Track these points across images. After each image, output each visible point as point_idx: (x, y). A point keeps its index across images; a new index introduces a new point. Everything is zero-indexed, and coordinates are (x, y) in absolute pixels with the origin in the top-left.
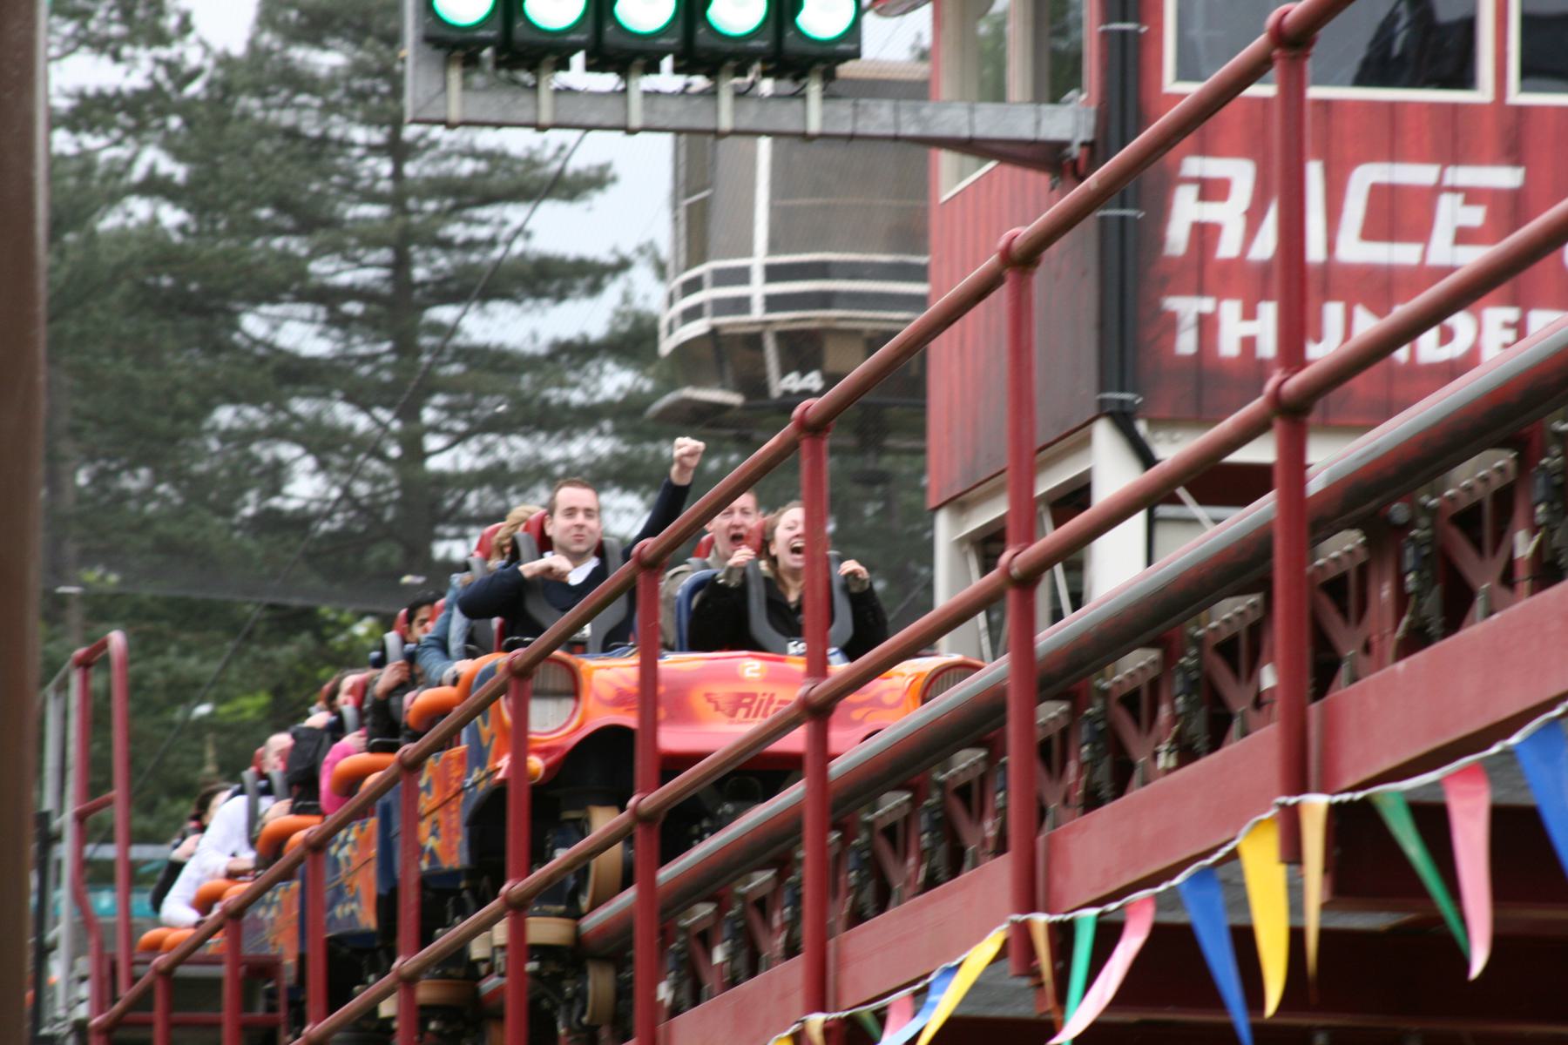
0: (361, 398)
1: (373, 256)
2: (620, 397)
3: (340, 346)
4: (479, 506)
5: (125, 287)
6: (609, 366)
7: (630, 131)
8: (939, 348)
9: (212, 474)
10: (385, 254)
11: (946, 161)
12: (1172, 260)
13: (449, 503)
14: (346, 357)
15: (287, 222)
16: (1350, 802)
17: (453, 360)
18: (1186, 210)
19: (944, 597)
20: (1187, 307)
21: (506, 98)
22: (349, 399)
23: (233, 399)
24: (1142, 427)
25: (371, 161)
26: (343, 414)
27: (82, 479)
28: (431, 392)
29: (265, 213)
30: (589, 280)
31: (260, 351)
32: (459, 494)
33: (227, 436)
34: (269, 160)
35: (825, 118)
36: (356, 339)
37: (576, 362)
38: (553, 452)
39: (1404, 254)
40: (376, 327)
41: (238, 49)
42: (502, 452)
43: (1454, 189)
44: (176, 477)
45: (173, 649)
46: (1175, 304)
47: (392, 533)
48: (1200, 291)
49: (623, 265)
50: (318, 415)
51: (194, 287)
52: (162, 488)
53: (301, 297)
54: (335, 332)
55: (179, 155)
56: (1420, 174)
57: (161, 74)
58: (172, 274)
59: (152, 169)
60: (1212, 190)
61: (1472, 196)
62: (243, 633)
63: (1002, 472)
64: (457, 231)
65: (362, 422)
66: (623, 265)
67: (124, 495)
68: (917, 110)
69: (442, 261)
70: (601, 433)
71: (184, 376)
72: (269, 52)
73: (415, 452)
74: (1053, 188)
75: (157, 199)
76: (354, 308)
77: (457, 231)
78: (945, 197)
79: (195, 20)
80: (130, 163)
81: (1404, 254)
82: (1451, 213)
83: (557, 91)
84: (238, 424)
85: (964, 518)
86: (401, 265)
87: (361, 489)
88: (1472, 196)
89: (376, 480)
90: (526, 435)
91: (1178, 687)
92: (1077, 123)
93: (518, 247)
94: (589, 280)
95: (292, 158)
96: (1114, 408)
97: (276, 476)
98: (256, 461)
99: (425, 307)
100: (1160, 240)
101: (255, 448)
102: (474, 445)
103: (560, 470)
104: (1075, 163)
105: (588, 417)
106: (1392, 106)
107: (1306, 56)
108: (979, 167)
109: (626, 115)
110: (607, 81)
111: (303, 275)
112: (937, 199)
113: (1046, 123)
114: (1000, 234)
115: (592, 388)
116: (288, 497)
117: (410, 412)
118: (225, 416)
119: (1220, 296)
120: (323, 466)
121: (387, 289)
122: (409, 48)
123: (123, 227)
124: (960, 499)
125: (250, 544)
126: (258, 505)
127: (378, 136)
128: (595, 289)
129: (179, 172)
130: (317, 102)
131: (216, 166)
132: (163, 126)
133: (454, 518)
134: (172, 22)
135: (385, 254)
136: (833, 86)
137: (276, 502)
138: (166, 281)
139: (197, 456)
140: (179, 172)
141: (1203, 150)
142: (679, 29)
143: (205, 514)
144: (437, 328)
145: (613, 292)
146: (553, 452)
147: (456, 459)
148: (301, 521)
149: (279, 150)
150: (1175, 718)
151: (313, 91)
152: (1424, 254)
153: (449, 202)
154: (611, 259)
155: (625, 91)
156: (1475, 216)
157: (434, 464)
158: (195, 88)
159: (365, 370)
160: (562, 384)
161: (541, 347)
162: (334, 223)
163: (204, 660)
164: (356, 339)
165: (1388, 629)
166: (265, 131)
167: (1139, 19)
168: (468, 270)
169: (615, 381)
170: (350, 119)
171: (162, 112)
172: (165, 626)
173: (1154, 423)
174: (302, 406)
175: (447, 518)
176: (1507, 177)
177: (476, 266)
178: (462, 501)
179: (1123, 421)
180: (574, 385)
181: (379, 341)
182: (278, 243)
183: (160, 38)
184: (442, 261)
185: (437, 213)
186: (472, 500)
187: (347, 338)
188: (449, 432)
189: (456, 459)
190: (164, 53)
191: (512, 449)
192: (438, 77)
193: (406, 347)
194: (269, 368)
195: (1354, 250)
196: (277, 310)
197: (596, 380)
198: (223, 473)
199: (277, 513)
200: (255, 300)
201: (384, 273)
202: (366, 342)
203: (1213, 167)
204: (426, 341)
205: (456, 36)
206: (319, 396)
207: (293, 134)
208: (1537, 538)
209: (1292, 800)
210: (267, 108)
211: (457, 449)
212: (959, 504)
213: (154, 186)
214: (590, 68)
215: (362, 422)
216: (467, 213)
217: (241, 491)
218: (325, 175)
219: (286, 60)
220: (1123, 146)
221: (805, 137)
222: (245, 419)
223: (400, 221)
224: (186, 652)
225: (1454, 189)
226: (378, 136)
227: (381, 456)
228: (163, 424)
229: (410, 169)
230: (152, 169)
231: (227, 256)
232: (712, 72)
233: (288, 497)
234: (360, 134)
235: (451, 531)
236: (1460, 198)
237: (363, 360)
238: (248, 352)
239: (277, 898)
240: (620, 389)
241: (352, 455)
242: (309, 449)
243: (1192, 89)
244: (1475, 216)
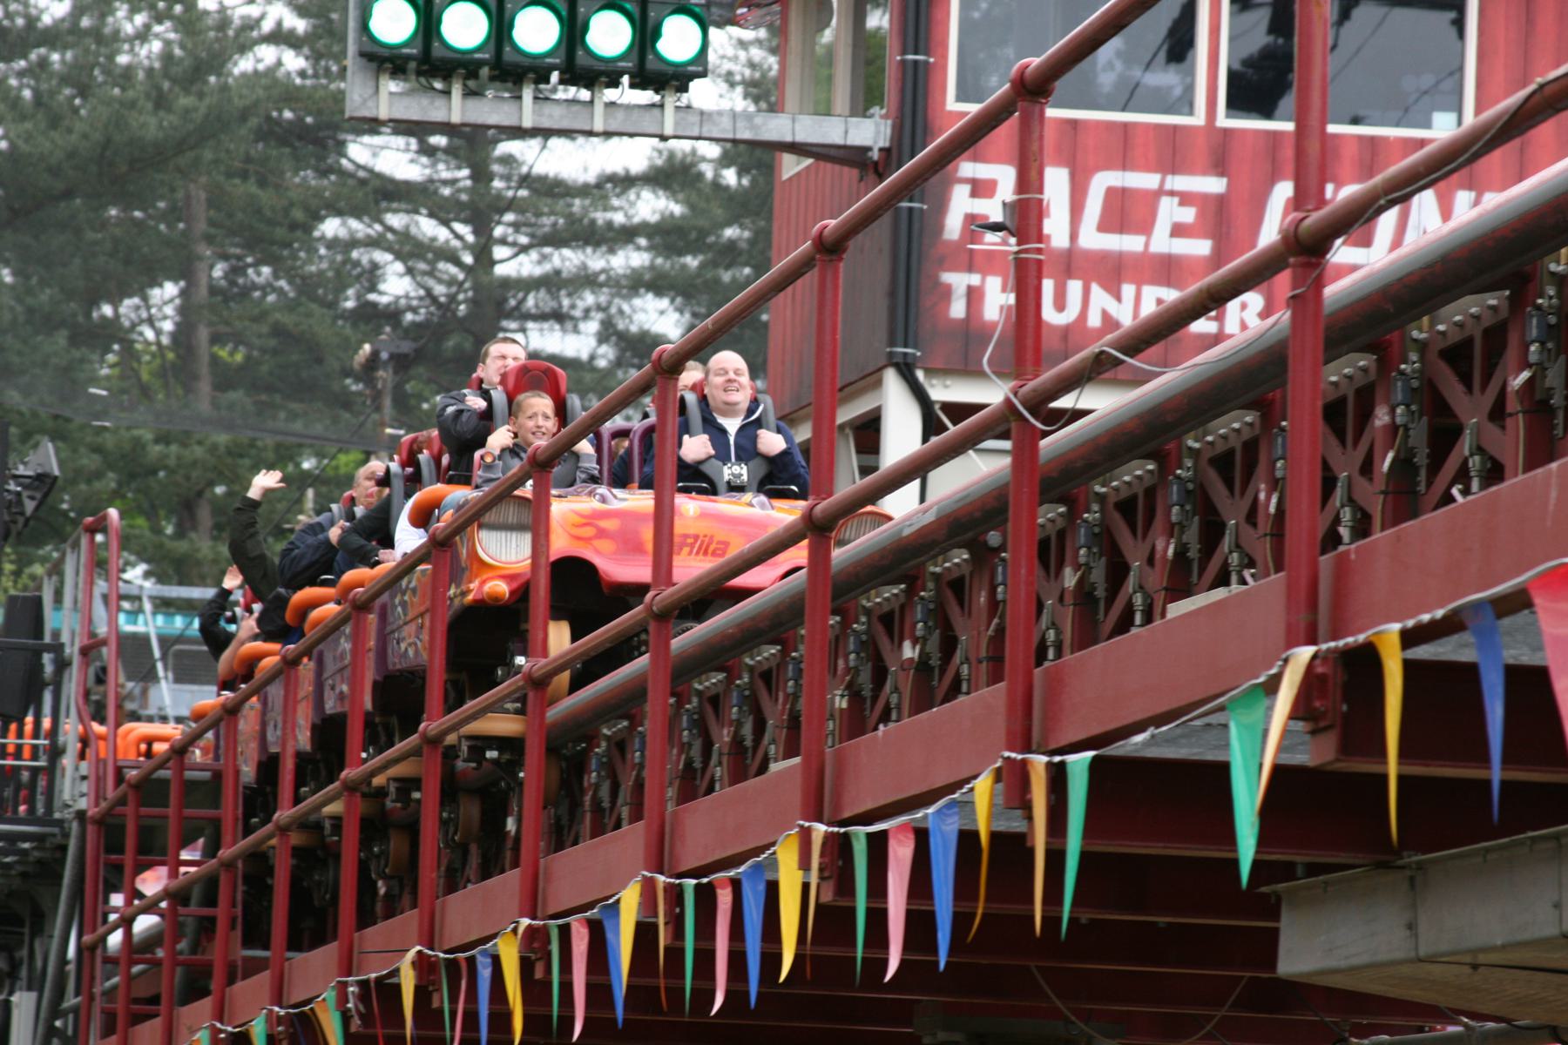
0: (443, 212)
4: (537, 306)
5: (254, 122)
9: (321, 273)
12: (950, 243)
13: (513, 302)
14: (431, 181)
16: (838, 833)
18: (961, 204)
20: (958, 281)
21: (425, 101)
23: (339, 213)
24: (920, 374)
26: (427, 228)
27: (218, 271)
31: (361, 174)
32: (520, 295)
33: (333, 244)
37: (618, 190)
39: (1131, 243)
40: (456, 156)
43: (1172, 193)
45: (282, 415)
46: (949, 277)
47: (463, 324)
48: (970, 269)
50: (407, 227)
51: (309, 120)
54: (424, 160)
56: (1145, 181)
58: (292, 110)
59: (279, 23)
60: (981, 189)
61: (1185, 199)
63: (810, 404)
65: (442, 234)
70: (639, 248)
73: (484, 257)
74: (861, 180)
75: (283, 47)
78: (785, 176)
80: (263, 17)
81: (1131, 243)
82: (1170, 212)
87: (440, 290)
88: (1185, 199)
89: (452, 282)
91: (852, 647)
92: (878, 133)
96: (899, 360)
97: (372, 276)
98: (357, 263)
100: (940, 227)
101: (355, 254)
102: (534, 255)
103: (602, 278)
104: (876, 164)
105: (627, 235)
106: (1126, 126)
107: (841, 259)
108: (798, 164)
109: (520, 118)
112: (780, 176)
113: (852, 132)
116: (381, 293)
117: (482, 227)
118: (331, 227)
119: (985, 273)
120: (410, 271)
122: (351, 60)
123: (256, 72)
129: (300, 25)
138: (288, 114)
140: (300, 25)
141: (976, 159)
142: (562, 52)
148: (392, 315)
150: (848, 670)
152: (1147, 245)
156: (1188, 215)
157: (499, 270)
159: (446, 191)
160: (607, 208)
161: (591, 177)
164: (441, 166)
165: (982, 628)
167: (927, 54)
169: (650, 206)
172: (278, 398)
173: (930, 372)
174: (396, 220)
175: (509, 315)
176: (1214, 185)
178: (524, 299)
179: (906, 371)
180: (615, 209)
181: (459, 168)
186: (530, 302)
187: (434, 165)
188: (514, 244)
191: (563, 259)
192: (371, 83)
193: (481, 175)
194: (369, 188)
195: (1093, 239)
198: (330, 274)
199: (374, 305)
203: (982, 171)
204: (496, 168)
205: (386, 53)
206: (408, 212)
208: (1079, 573)
209: (807, 824)
211: (522, 257)
213: (280, 37)
215: (442, 234)
217: (345, 287)
220: (912, 157)
222: (350, 229)
224: (293, 416)
225: (1172, 193)
227: (457, 262)
228: (280, 233)
232: (589, 85)
233: (381, 293)
235: (513, 325)
236: (1176, 200)
237: (445, 182)
238: (352, 175)
239: (413, 585)
242: (399, 256)
243: (973, 108)
244: (1188, 215)
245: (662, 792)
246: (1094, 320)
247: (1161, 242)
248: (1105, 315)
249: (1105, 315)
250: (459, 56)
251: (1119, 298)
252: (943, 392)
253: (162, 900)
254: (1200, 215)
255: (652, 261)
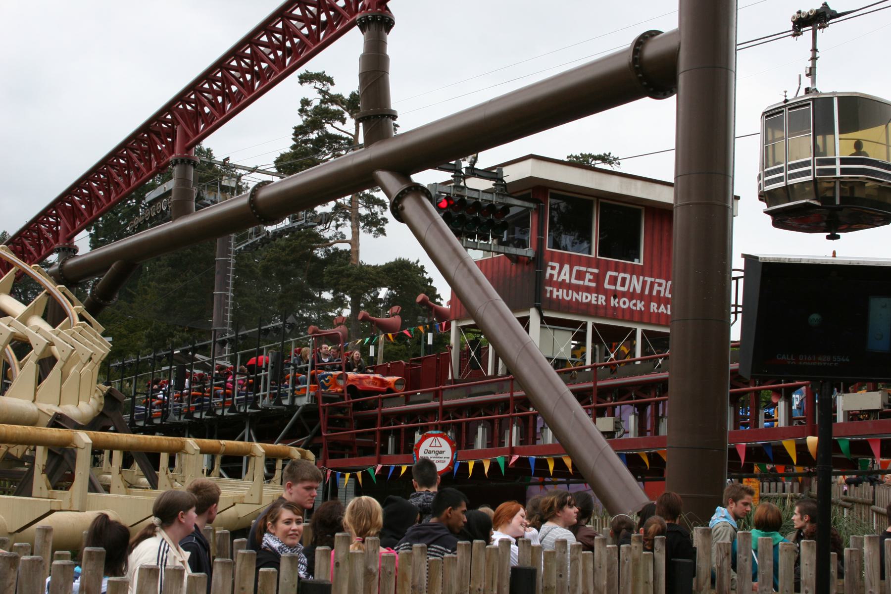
20: (549, 289)
39: (581, 283)
61: (591, 273)
81: (581, 283)
82: (588, 276)
88: (591, 273)
156: (591, 277)
176: (596, 271)
195: (574, 281)
203: (553, 264)
245: (380, 406)
246: (574, 300)
247: (587, 283)
248: (576, 298)
249: (576, 298)
250: (731, 175)
251: (576, 298)
252: (546, 314)
253: (556, 434)
254: (594, 277)
255: (320, 294)
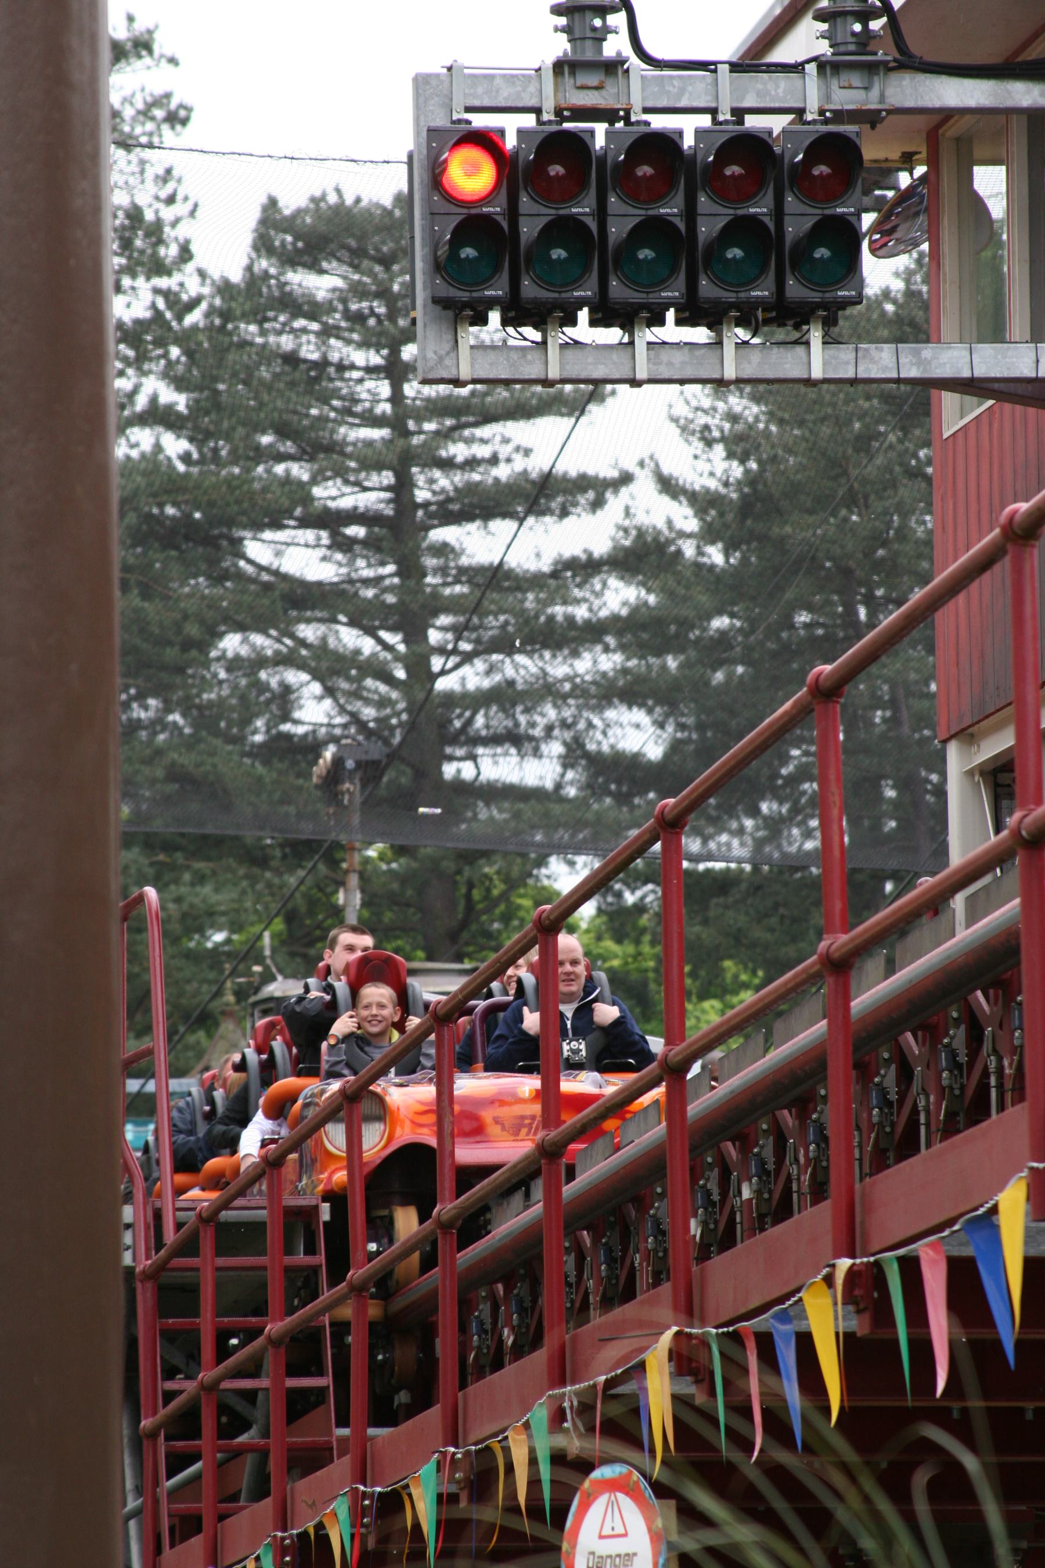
1: (375, 479)
2: (624, 612)
3: (344, 570)
6: (613, 582)
7: (635, 383)
8: (945, 618)
9: (221, 701)
10: (388, 477)
11: (949, 400)
13: (457, 724)
15: (288, 447)
17: (457, 581)
19: (957, 856)
22: (352, 623)
23: (241, 627)
25: (370, 384)
28: (435, 614)
29: (266, 439)
30: (591, 495)
33: (234, 664)
34: (270, 387)
35: (825, 364)
36: (361, 563)
38: (558, 668)
40: (379, 549)
41: (236, 276)
42: (510, 672)
44: (187, 707)
45: (187, 877)
49: (626, 478)
50: (324, 639)
52: (176, 717)
53: (304, 523)
54: (339, 556)
55: (180, 384)
57: (161, 304)
59: (154, 399)
62: (257, 858)
64: (459, 451)
65: (367, 645)
66: (626, 478)
67: (136, 725)
68: (917, 353)
69: (444, 481)
70: (607, 649)
71: (191, 606)
72: (266, 275)
76: (357, 531)
77: (459, 451)
79: (193, 248)
83: (565, 346)
84: (244, 651)
85: (974, 749)
86: (402, 488)
89: (383, 702)
90: (530, 654)
93: (520, 464)
94: (591, 495)
95: (292, 384)
98: (264, 687)
99: (428, 528)
101: (263, 675)
102: (480, 665)
110: (613, 335)
111: (307, 499)
114: (1003, 508)
115: (597, 603)
117: (415, 633)
118: (231, 643)
120: (330, 692)
121: (389, 511)
124: (970, 730)
125: (260, 769)
126: (268, 731)
127: (375, 359)
128: (597, 504)
129: (181, 401)
130: (315, 326)
131: (216, 392)
132: (166, 355)
133: (463, 738)
134: (171, 251)
135: (388, 477)
136: (835, 331)
137: (286, 727)
138: (170, 511)
139: (205, 684)
140: (181, 401)
143: (218, 742)
144: (443, 550)
145: (615, 504)
146: (558, 668)
147: (463, 679)
149: (276, 376)
151: (312, 317)
153: (449, 422)
154: (614, 474)
155: (632, 343)
157: (442, 684)
158: (194, 318)
159: (370, 593)
162: (334, 448)
163: (217, 890)
166: (266, 354)
168: (471, 488)
170: (348, 342)
171: (161, 342)
172: (179, 857)
175: (455, 739)
177: (478, 484)
178: (470, 721)
180: (577, 602)
181: (383, 564)
182: (280, 469)
183: (158, 268)
184: (444, 481)
185: (437, 433)
187: (351, 563)
189: (463, 679)
190: (163, 282)
191: (516, 666)
196: (281, 536)
197: (598, 595)
199: (288, 737)
200: (258, 527)
201: (388, 495)
202: (369, 565)
204: (430, 562)
207: (292, 359)
210: (263, 333)
212: (968, 735)
214: (593, 323)
215: (367, 645)
216: (467, 432)
218: (324, 400)
219: (282, 285)
221: (809, 382)
222: (253, 646)
223: (401, 442)
224: (200, 879)
226: (375, 359)
227: (388, 679)
228: (171, 654)
229: (410, 389)
230: (154, 399)
231: (230, 482)
234: (360, 357)
235: (460, 752)
237: (366, 582)
240: (625, 604)
241: (359, 679)
242: (316, 676)
